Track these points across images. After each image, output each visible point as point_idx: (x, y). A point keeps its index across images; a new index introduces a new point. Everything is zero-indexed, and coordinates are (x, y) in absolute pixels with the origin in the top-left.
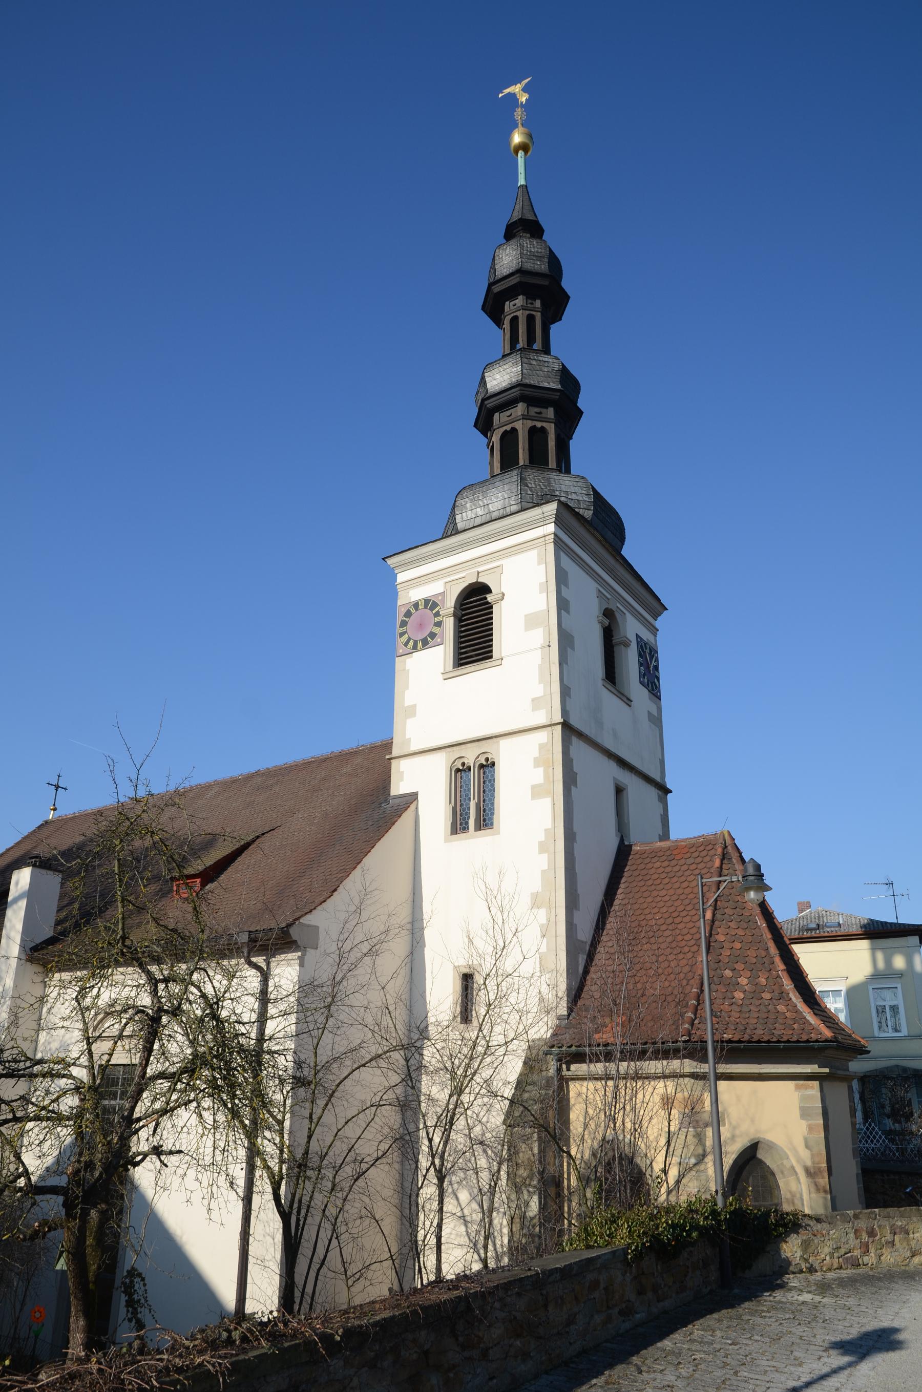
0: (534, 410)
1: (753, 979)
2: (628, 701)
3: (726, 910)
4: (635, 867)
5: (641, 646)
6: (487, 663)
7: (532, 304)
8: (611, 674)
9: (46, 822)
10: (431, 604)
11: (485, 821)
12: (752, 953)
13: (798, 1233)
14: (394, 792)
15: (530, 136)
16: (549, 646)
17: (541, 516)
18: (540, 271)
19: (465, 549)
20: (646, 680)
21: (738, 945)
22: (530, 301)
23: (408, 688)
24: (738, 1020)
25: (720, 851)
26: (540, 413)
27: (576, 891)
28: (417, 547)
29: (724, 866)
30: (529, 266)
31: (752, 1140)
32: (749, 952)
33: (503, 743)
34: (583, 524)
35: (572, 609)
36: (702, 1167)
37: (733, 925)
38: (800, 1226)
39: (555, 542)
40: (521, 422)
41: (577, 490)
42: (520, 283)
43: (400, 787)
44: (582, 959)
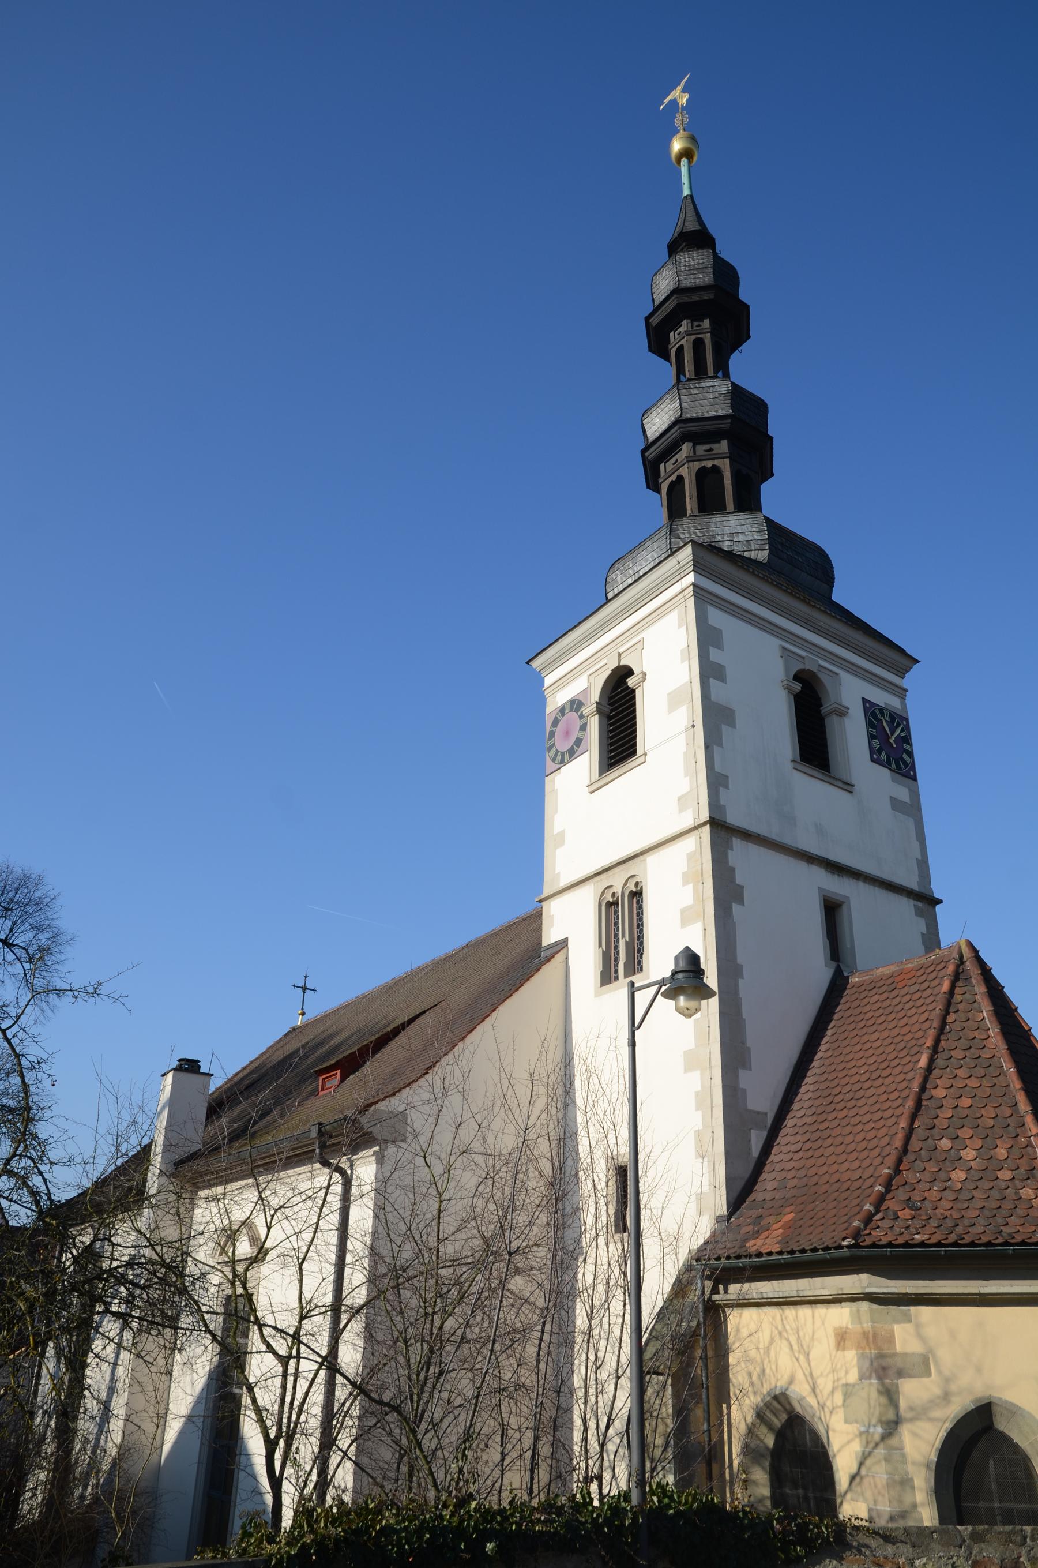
0: (701, 449)
1: (986, 1152)
2: (847, 786)
3: (953, 1053)
4: (848, 1005)
5: (874, 714)
6: (631, 763)
7: (699, 326)
8: (814, 748)
9: (294, 1029)
10: (576, 705)
11: (641, 970)
12: (989, 1112)
13: (840, 1559)
14: (545, 943)
15: (692, 139)
16: (693, 726)
17: (677, 567)
18: (702, 284)
19: (606, 630)
20: (883, 756)
21: (966, 1102)
22: (695, 324)
23: (556, 812)
24: (948, 1213)
25: (951, 968)
26: (711, 450)
27: (744, 1043)
28: (557, 640)
29: (957, 990)
30: (688, 282)
31: (978, 1400)
32: (983, 1112)
33: (651, 859)
34: (742, 567)
35: (729, 674)
36: (893, 1441)
37: (962, 1073)
38: (848, 1546)
39: (696, 594)
40: (686, 466)
41: (745, 528)
42: (678, 305)
43: (550, 936)
44: (757, 1140)
